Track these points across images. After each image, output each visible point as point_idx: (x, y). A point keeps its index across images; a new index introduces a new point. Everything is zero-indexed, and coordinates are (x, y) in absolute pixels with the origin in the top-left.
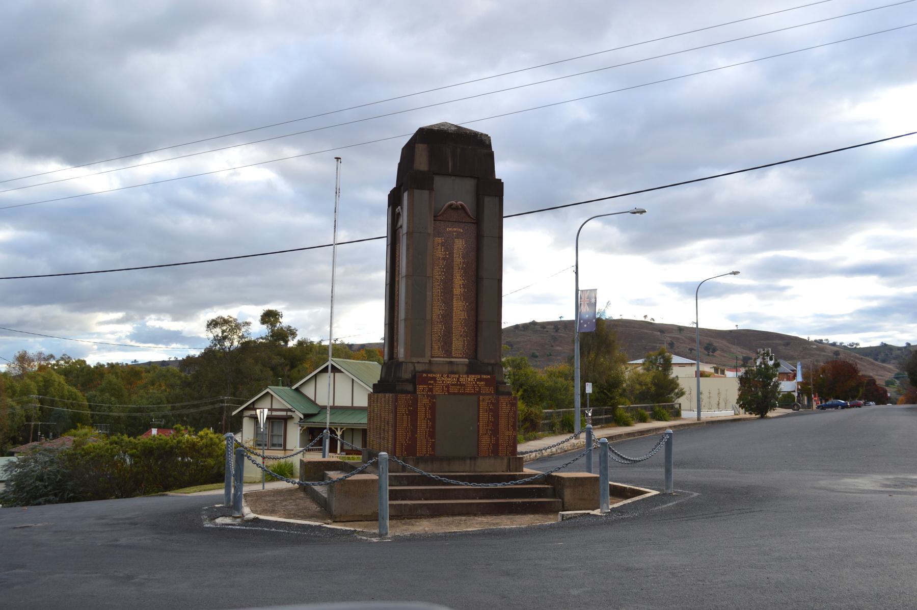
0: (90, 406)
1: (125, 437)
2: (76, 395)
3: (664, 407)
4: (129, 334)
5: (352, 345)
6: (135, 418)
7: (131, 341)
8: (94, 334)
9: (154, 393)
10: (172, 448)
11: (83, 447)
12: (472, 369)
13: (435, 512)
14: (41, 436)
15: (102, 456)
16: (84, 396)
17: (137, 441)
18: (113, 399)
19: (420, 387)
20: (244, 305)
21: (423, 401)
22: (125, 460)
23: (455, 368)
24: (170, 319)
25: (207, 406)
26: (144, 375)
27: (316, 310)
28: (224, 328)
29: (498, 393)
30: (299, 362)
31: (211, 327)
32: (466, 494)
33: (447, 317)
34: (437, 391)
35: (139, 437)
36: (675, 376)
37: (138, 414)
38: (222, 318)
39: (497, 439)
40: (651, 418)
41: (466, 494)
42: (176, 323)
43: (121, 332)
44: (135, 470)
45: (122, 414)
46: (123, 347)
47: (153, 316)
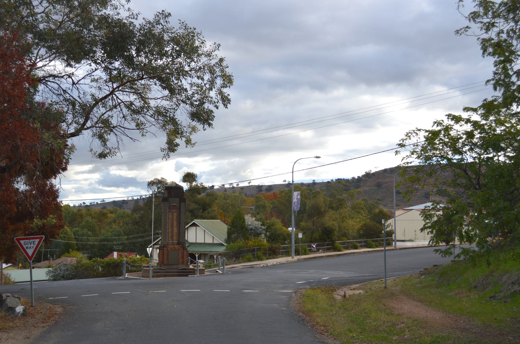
0: (75, 238)
1: (99, 259)
2: (66, 231)
3: (373, 241)
4: (97, 180)
5: (262, 186)
6: (104, 245)
7: (99, 186)
8: (71, 181)
9: (116, 228)
10: (118, 263)
11: (81, 263)
12: (178, 244)
13: (165, 276)
14: (50, 257)
15: (89, 267)
16: (71, 231)
17: (103, 260)
18: (89, 233)
19: (165, 248)
20: (179, 157)
21: (166, 252)
22: (99, 269)
23: (174, 244)
24: (127, 169)
25: (149, 236)
26: (109, 215)
27: (233, 160)
28: (159, 186)
29: (184, 249)
30: (208, 207)
31: (150, 185)
32: (173, 272)
33: (172, 232)
34: (169, 249)
35: (105, 259)
36: (389, 223)
37: (106, 243)
38: (157, 179)
39: (183, 260)
40: (344, 249)
41: (173, 272)
42: (131, 172)
43: (92, 179)
44: (103, 273)
45: (96, 243)
46: (94, 191)
47: (114, 167)
